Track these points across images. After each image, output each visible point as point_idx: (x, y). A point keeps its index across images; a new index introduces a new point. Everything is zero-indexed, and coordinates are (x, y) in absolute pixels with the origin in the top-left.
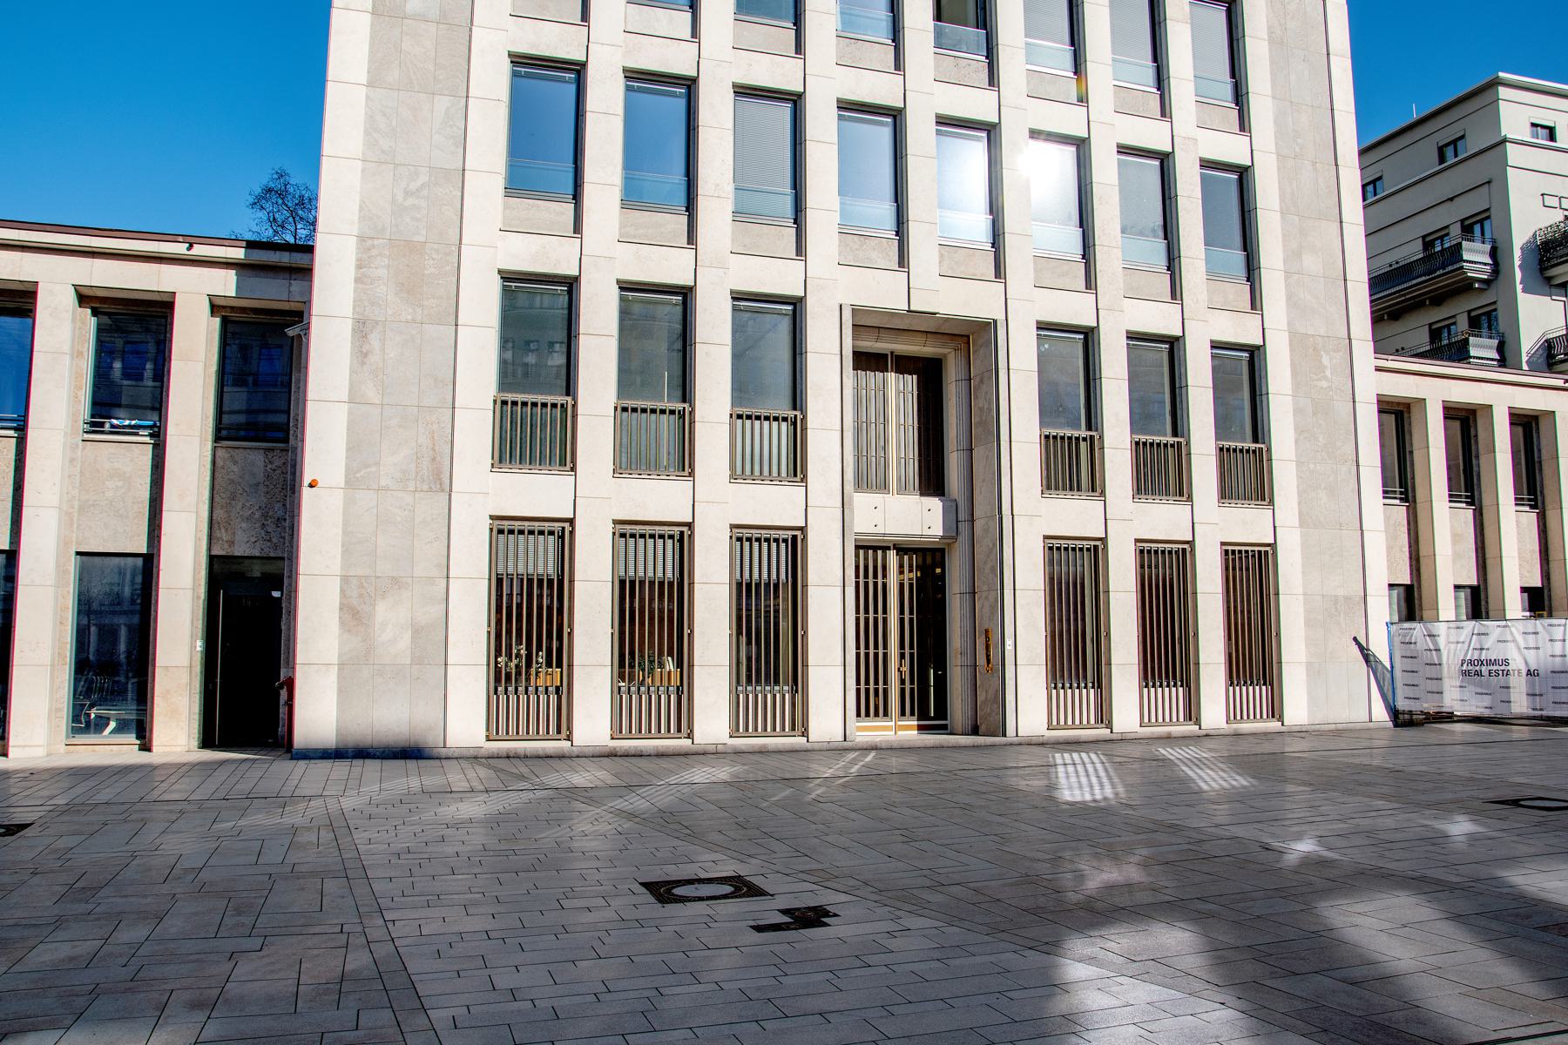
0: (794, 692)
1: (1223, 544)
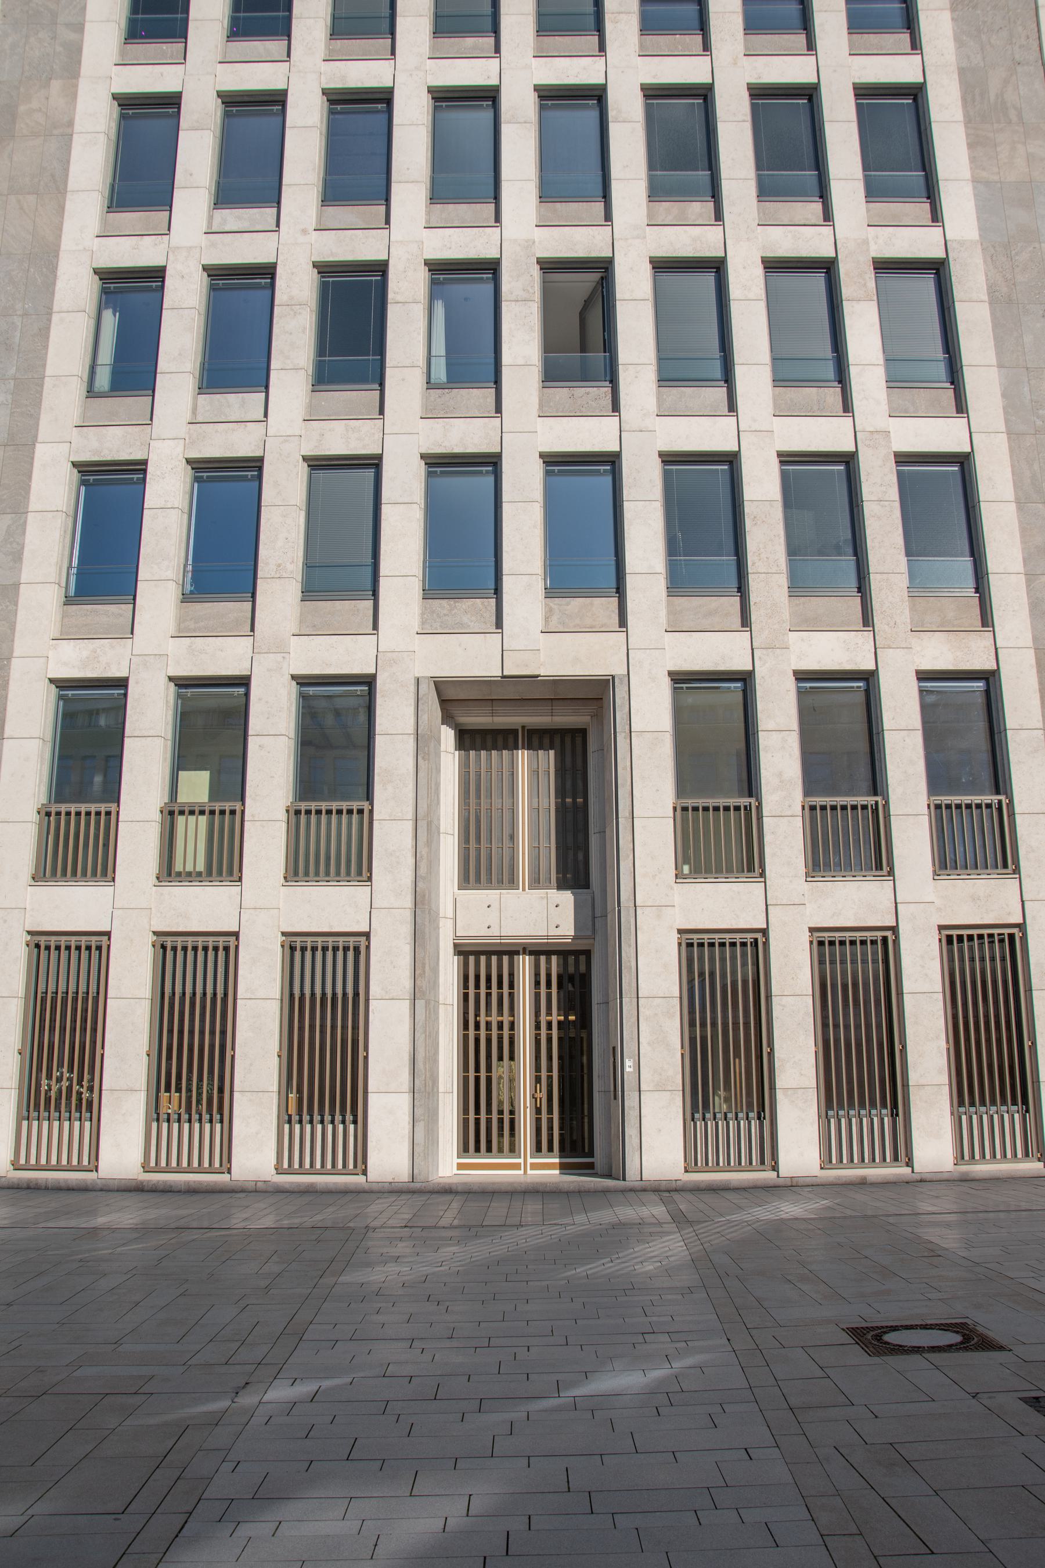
0: (894, 1115)
1: (941, 928)
